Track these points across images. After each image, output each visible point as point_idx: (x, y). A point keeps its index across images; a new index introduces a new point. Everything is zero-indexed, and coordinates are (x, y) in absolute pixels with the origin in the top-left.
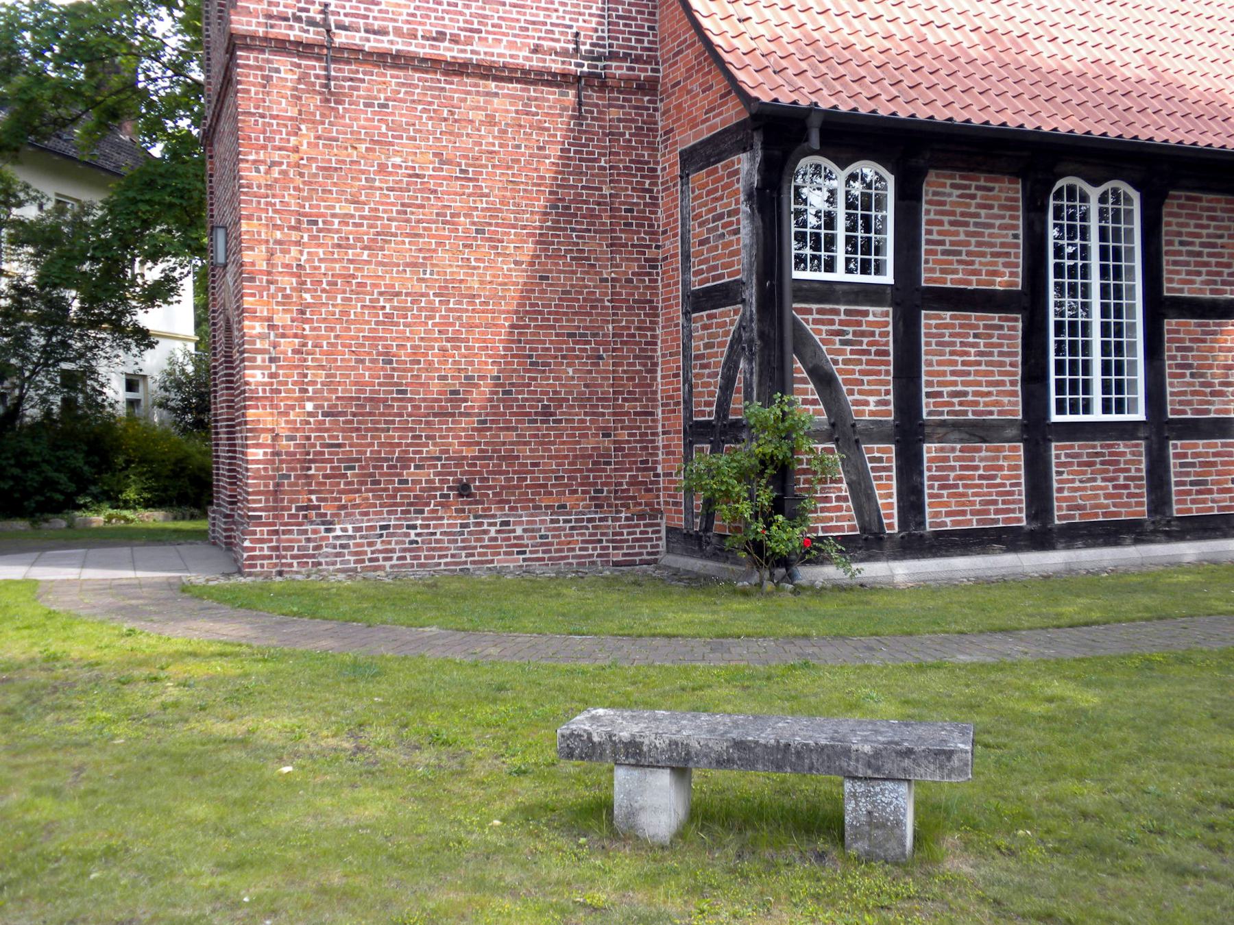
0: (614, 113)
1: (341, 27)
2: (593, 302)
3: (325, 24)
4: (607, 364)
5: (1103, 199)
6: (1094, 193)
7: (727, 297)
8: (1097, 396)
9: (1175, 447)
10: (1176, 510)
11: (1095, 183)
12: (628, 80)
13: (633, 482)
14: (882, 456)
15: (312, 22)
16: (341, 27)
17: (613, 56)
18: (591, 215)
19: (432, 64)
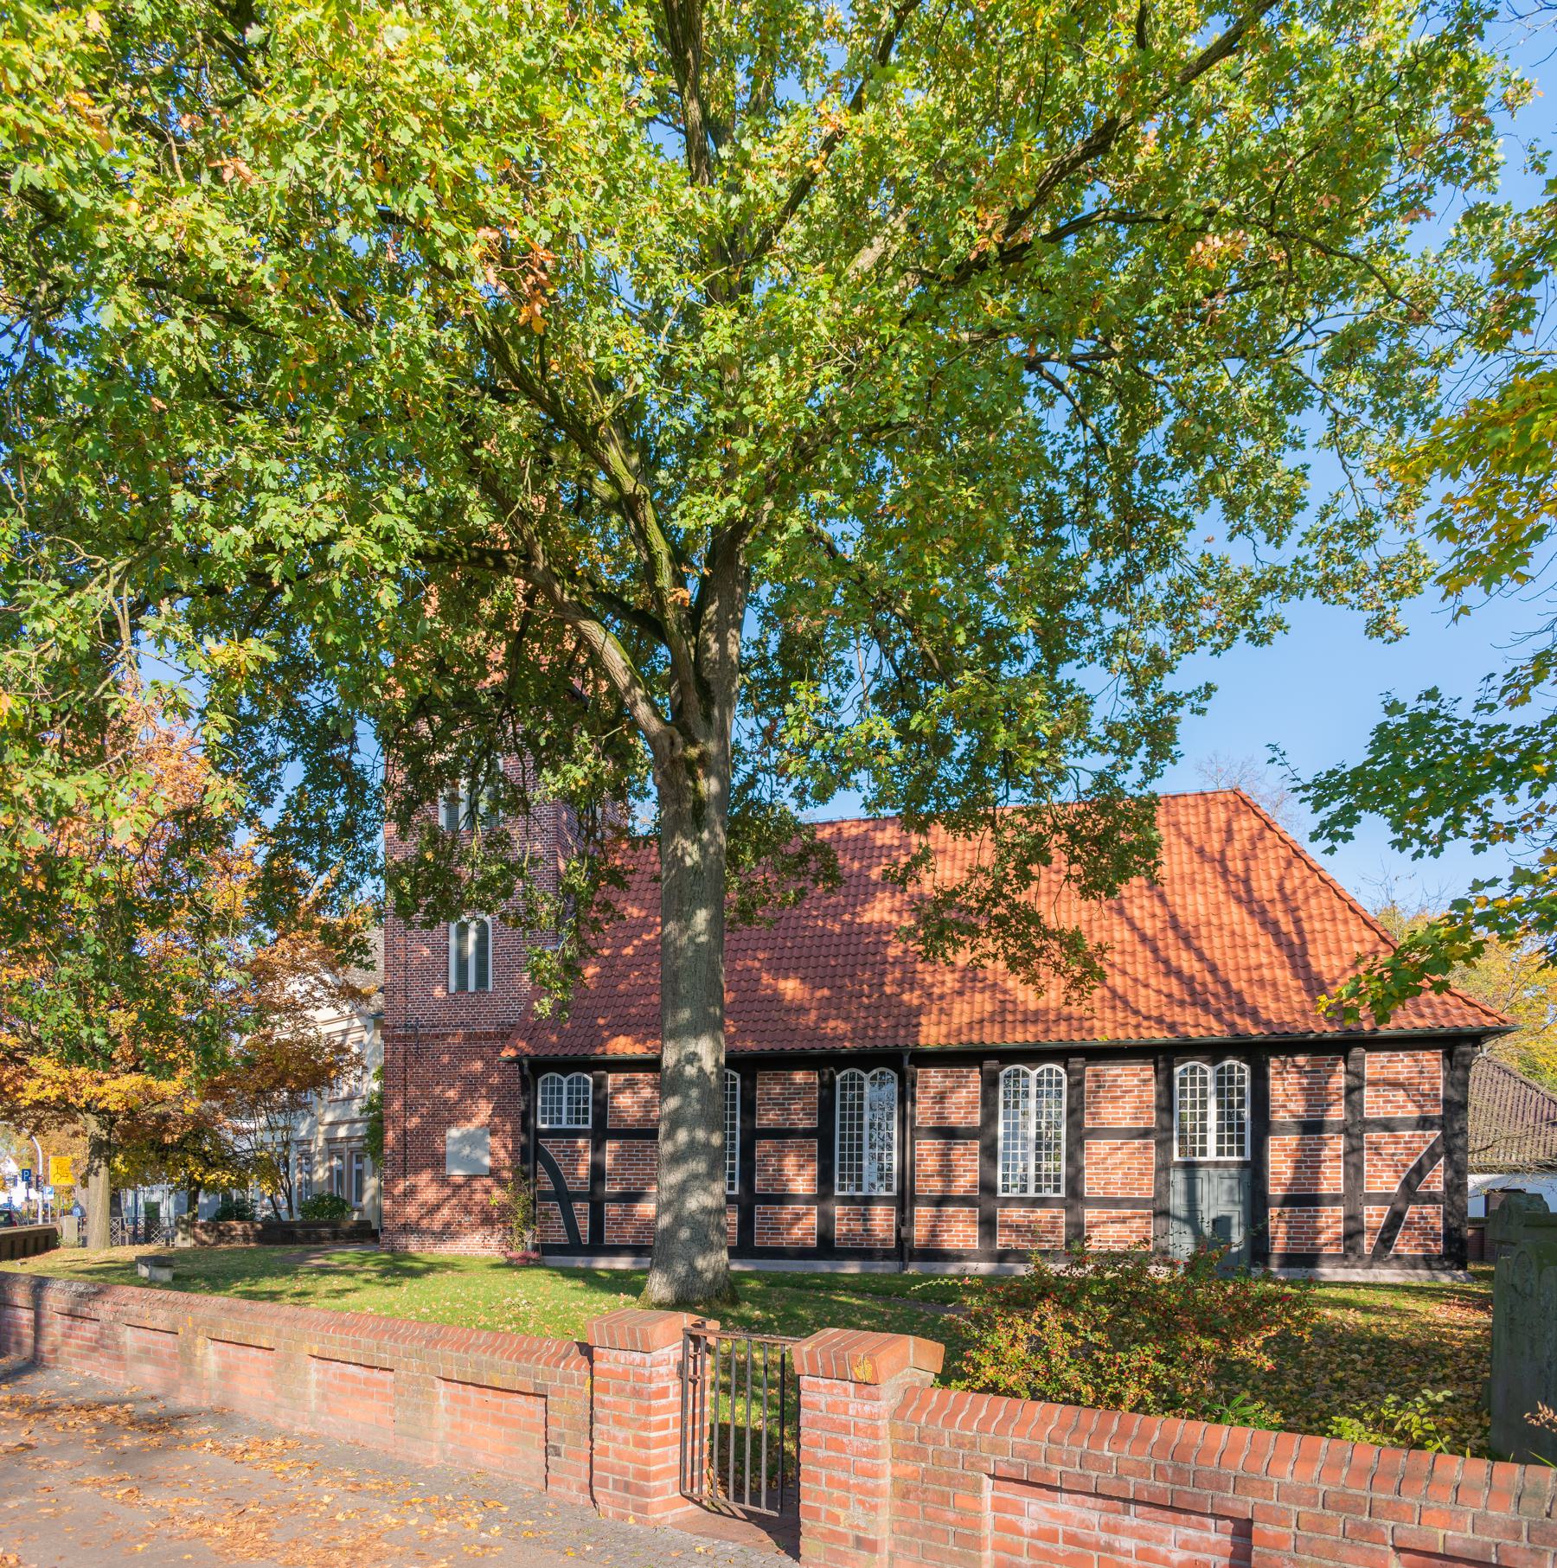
14: (581, 1208)
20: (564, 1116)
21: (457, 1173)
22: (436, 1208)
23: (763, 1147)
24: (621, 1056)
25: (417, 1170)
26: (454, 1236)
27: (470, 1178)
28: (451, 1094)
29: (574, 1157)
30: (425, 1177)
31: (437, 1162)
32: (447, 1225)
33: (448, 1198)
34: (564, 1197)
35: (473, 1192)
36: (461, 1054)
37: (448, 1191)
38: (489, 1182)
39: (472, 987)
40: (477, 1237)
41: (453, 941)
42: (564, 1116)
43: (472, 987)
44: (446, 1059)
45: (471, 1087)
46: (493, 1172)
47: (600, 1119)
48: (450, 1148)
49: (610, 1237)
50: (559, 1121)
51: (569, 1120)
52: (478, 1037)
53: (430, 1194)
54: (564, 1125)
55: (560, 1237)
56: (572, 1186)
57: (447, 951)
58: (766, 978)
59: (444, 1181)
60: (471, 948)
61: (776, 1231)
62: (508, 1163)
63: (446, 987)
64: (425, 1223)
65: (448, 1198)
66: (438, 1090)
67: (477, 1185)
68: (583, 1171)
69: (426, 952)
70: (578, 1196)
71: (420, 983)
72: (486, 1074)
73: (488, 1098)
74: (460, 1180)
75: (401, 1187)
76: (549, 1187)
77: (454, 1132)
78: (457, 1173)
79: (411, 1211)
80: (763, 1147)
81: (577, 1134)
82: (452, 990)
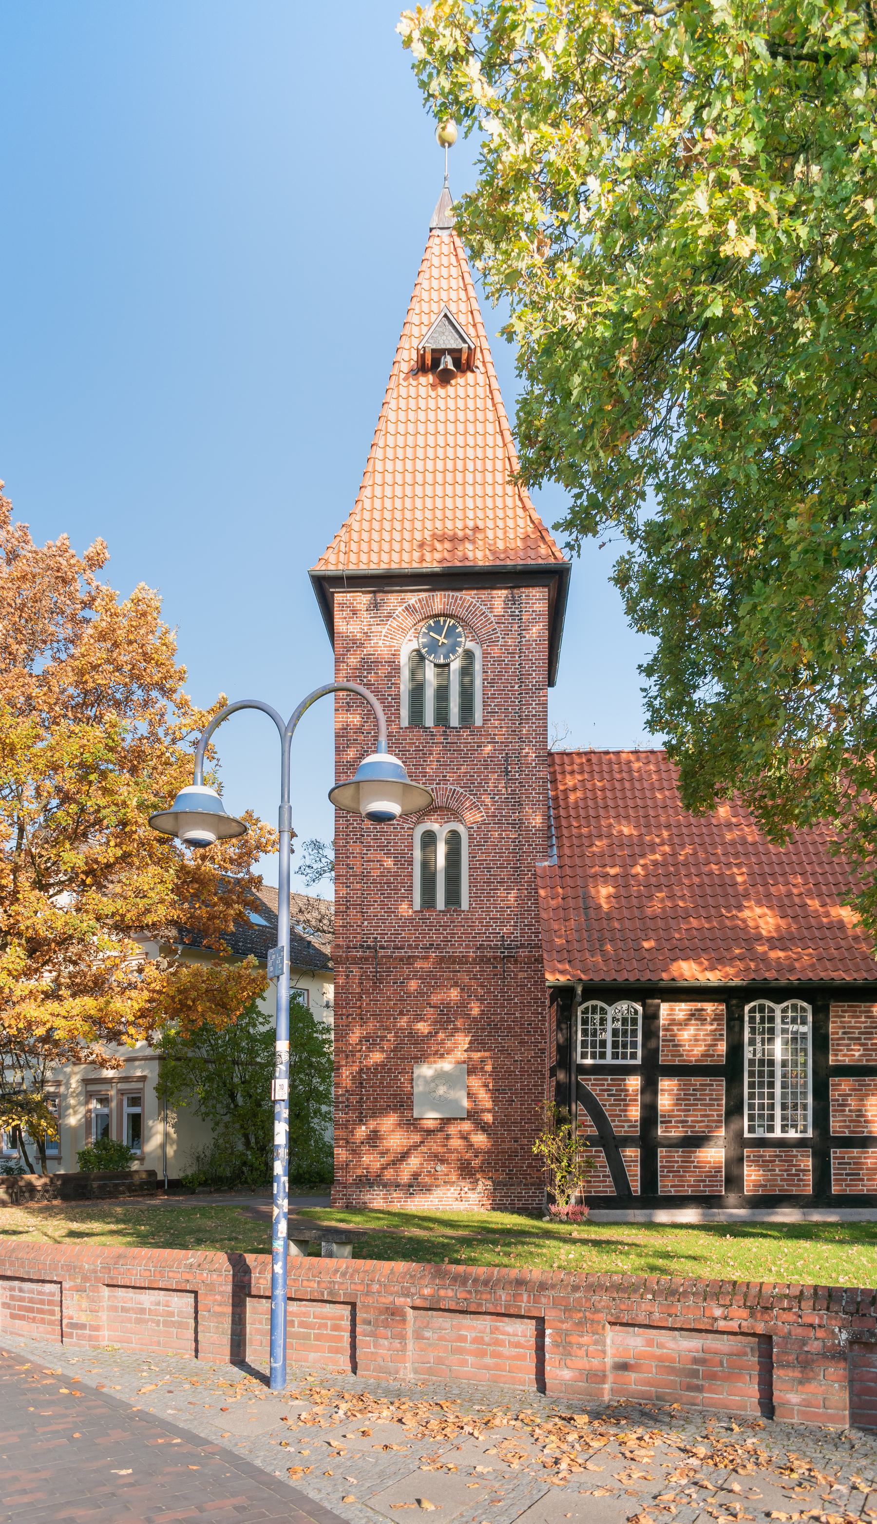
0: (521, 975)
1: (382, 947)
2: (510, 1072)
3: (375, 948)
4: (517, 1104)
5: (784, 1011)
6: (778, 1008)
7: (298, 1116)
8: (778, 1123)
9: (835, 1153)
10: (835, 1190)
11: (779, 1002)
12: (529, 957)
13: (530, 1166)
14: (631, 1154)
15: (369, 947)
16: (382, 947)
17: (522, 946)
18: (509, 1028)
19: (23, 1280)
20: (609, 1050)
21: (430, 1117)
22: (404, 1156)
23: (841, 1087)
24: (692, 983)
25: (378, 1112)
26: (427, 1189)
27: (446, 1121)
28: (423, 1027)
29: (621, 1098)
30: (388, 1122)
31: (402, 1103)
32: (416, 1175)
33: (416, 1146)
34: (609, 1142)
35: (448, 1137)
36: (432, 981)
37: (416, 1138)
38: (467, 1126)
39: (440, 904)
40: (453, 1191)
41: (417, 854)
42: (609, 1050)
43: (440, 904)
44: (413, 985)
45: (446, 1018)
46: (473, 1115)
47: (651, 1055)
48: (419, 1088)
49: (666, 1186)
50: (603, 1055)
51: (615, 1056)
52: (453, 960)
53: (396, 1141)
54: (609, 1060)
55: (608, 1188)
56: (620, 1129)
57: (411, 863)
58: (814, 904)
59: (412, 1124)
60: (441, 861)
61: (855, 1176)
62: (489, 1105)
63: (411, 905)
64: (389, 1174)
65: (416, 1146)
66: (403, 1022)
67: (452, 1130)
68: (635, 1113)
69: (389, 863)
70: (626, 1141)
71: (379, 897)
72: (463, 1005)
73: (467, 1031)
74: (430, 1124)
75: (362, 1131)
76: (593, 1131)
77: (425, 1071)
78: (430, 1117)
79: (371, 1161)
80: (841, 1087)
81: (628, 1070)
82: (417, 906)
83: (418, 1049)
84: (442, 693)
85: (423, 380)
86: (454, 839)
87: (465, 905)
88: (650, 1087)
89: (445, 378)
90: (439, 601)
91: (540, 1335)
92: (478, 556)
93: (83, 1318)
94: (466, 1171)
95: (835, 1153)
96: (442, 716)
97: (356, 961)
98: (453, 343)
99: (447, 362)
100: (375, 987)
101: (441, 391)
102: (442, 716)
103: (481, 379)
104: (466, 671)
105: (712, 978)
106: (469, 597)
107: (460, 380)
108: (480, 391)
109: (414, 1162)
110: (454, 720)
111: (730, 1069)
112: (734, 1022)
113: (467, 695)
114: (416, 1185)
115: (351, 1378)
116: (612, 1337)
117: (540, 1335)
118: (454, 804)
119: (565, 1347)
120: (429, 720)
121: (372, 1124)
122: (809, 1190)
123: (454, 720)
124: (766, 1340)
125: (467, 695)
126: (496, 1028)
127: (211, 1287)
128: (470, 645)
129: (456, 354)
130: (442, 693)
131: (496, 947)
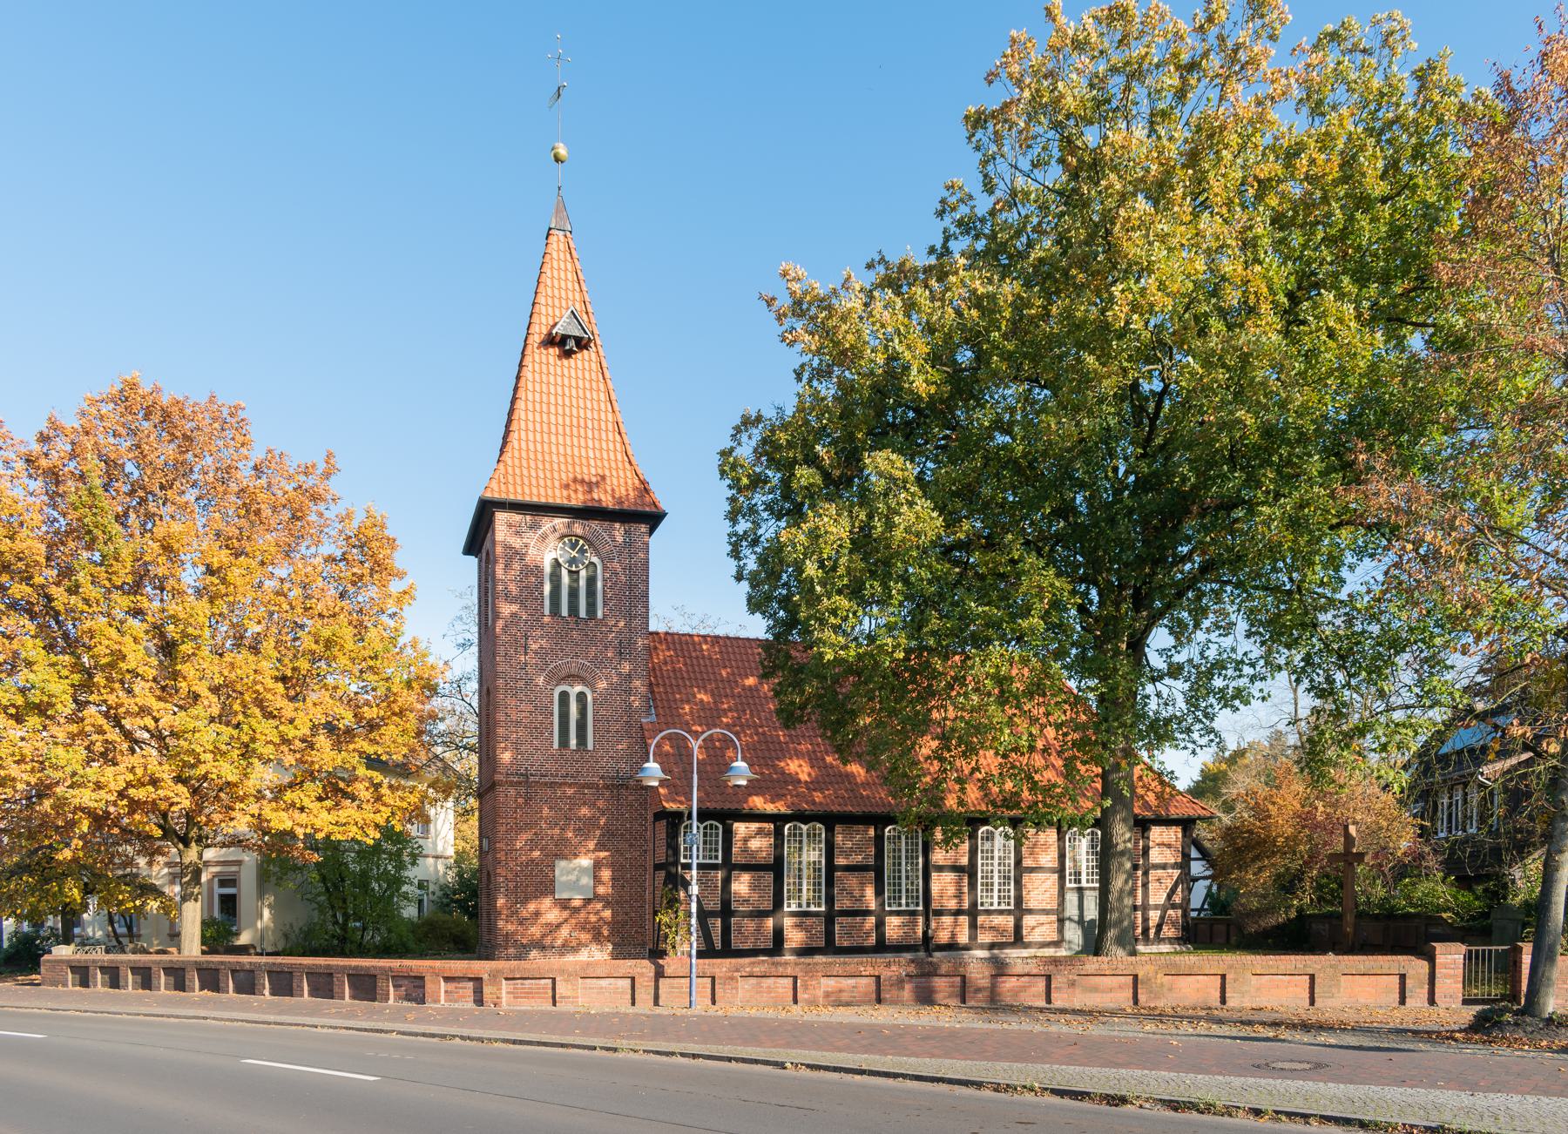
6: (805, 827)
9: (839, 919)
22: (559, 926)
37: (566, 914)
43: (573, 742)
45: (585, 829)
49: (736, 944)
59: (564, 904)
70: (713, 914)
74: (576, 903)
83: (563, 850)
84: (573, 593)
85: (551, 350)
86: (581, 697)
87: (590, 746)
88: (727, 882)
89: (568, 354)
90: (578, 528)
91: (795, 983)
92: (608, 502)
93: (569, 993)
94: (597, 938)
95: (839, 919)
96: (573, 609)
97: (512, 784)
98: (577, 333)
99: (571, 344)
100: (526, 803)
101: (565, 362)
102: (573, 609)
103: (594, 356)
104: (591, 581)
105: (770, 808)
106: (595, 525)
107: (579, 356)
108: (594, 366)
109: (564, 932)
110: (583, 614)
111: (776, 867)
112: (778, 834)
113: (591, 592)
114: (568, 948)
115: (631, 1010)
116: (823, 980)
117: (795, 983)
118: (583, 674)
119: (806, 987)
120: (565, 612)
121: (532, 907)
122: (823, 944)
123: (583, 614)
124: (878, 978)
125: (591, 592)
126: (613, 835)
127: (642, 975)
128: (595, 560)
129: (578, 340)
130: (573, 593)
131: (613, 778)
